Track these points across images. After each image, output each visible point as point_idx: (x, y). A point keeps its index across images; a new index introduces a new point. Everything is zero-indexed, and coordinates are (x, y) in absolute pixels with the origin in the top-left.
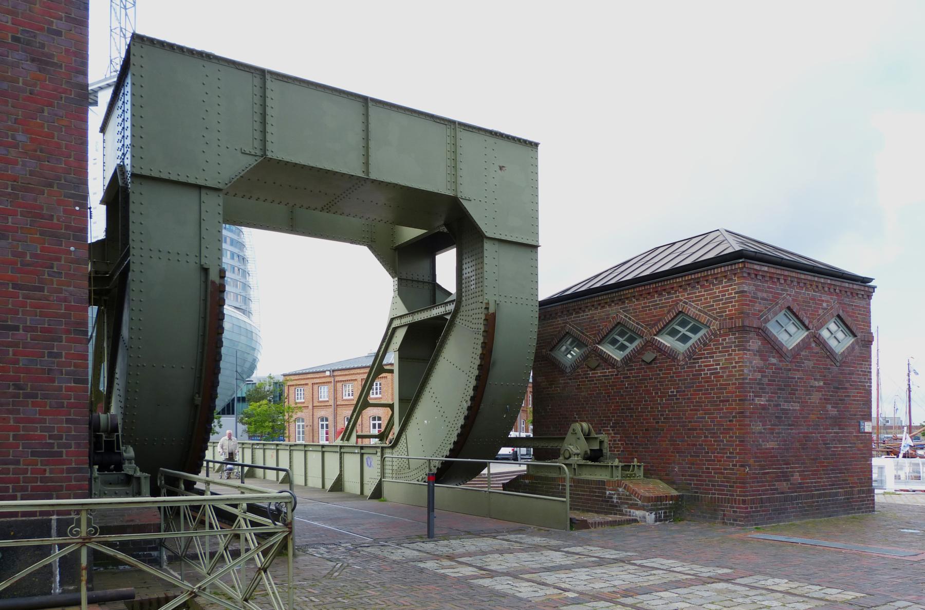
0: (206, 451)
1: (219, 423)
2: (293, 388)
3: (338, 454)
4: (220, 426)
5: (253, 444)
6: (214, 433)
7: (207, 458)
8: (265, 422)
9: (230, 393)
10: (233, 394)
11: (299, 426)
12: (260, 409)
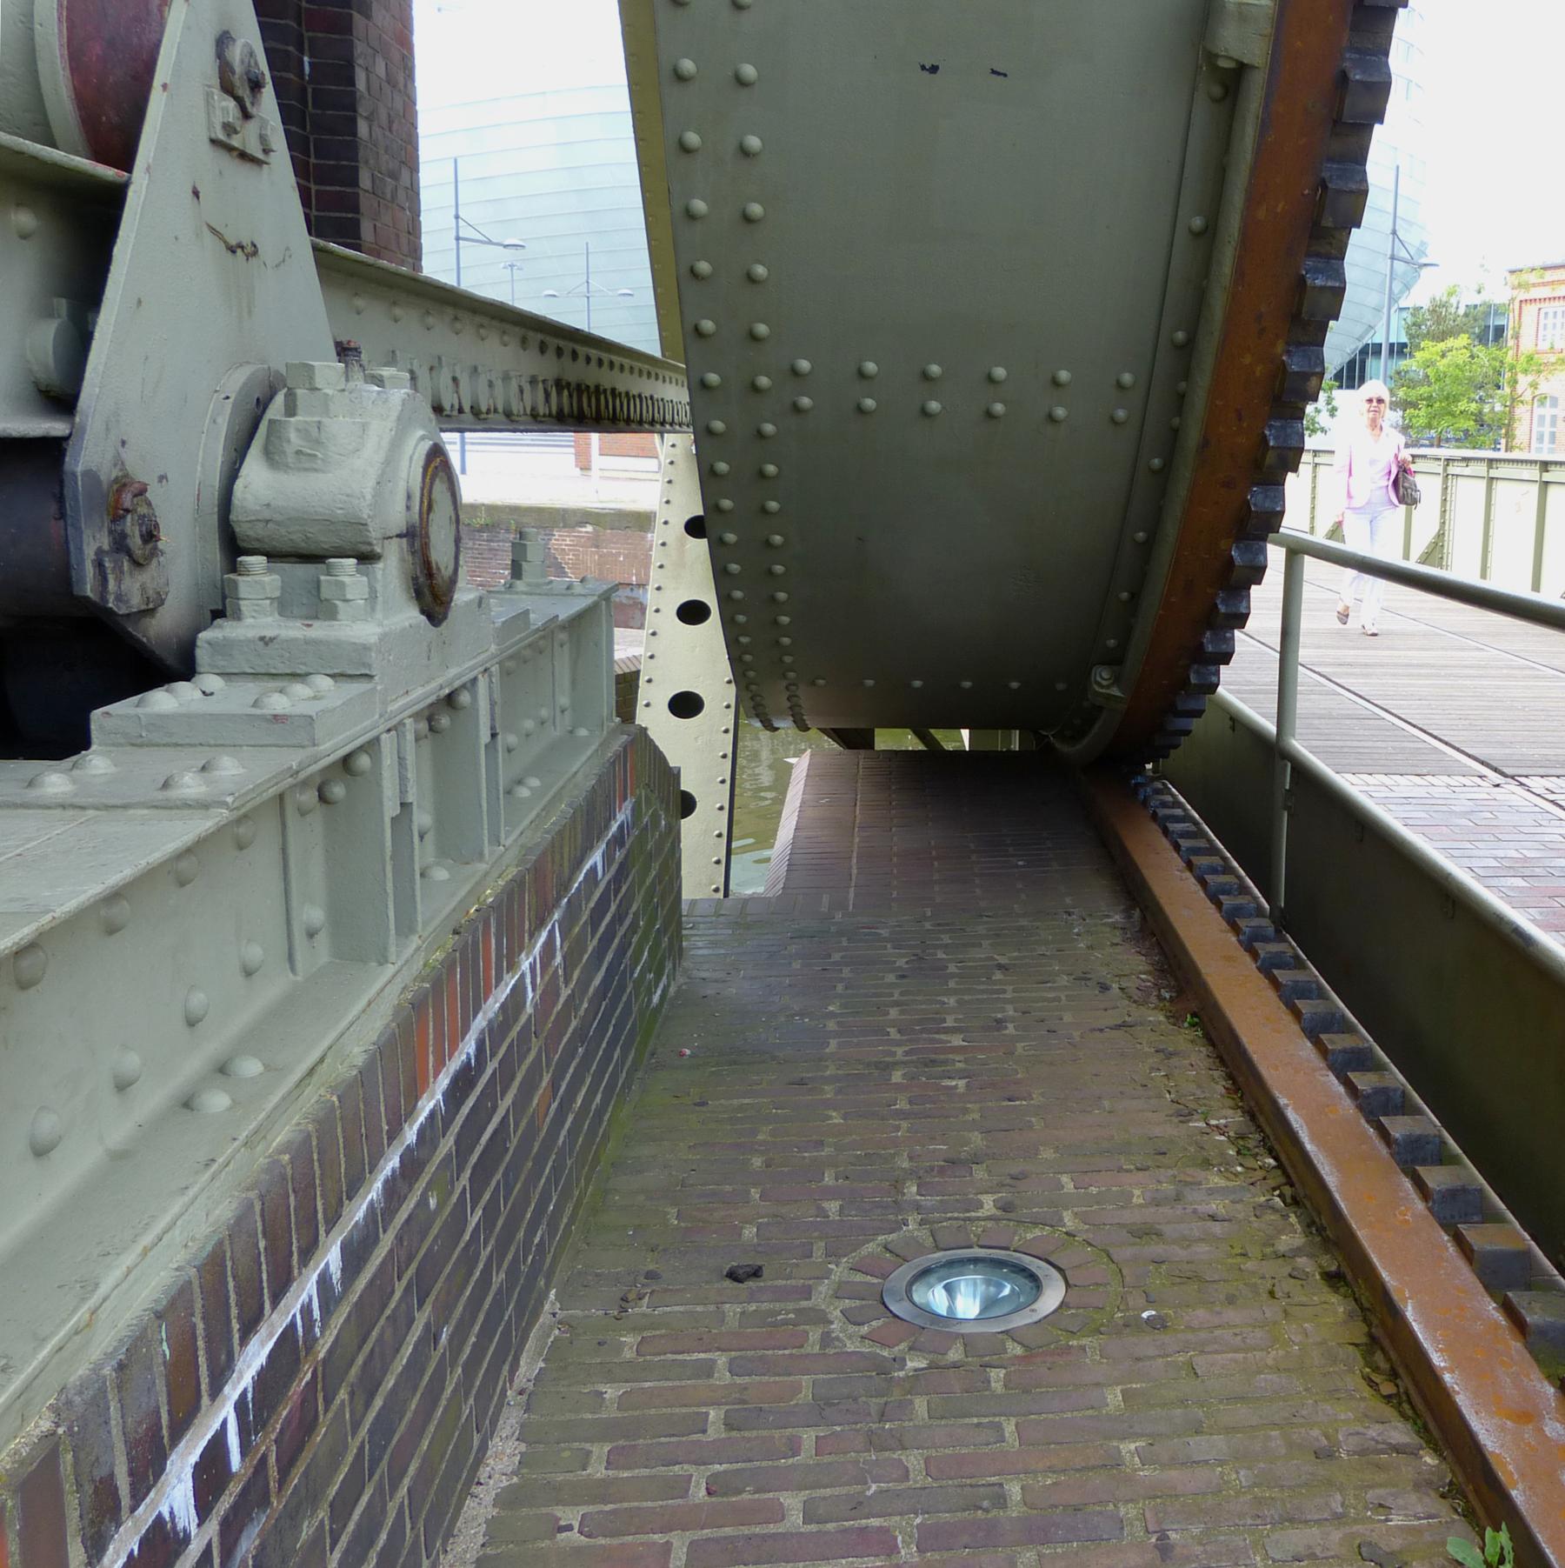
0: (1290, 476)
1: (1328, 404)
2: (1533, 308)
3: (1439, 480)
4: (1333, 412)
5: (1448, 461)
6: (1314, 431)
7: (1294, 521)
8: (1456, 400)
9: (1359, 330)
10: (1366, 332)
11: (1542, 418)
12: (1445, 361)
